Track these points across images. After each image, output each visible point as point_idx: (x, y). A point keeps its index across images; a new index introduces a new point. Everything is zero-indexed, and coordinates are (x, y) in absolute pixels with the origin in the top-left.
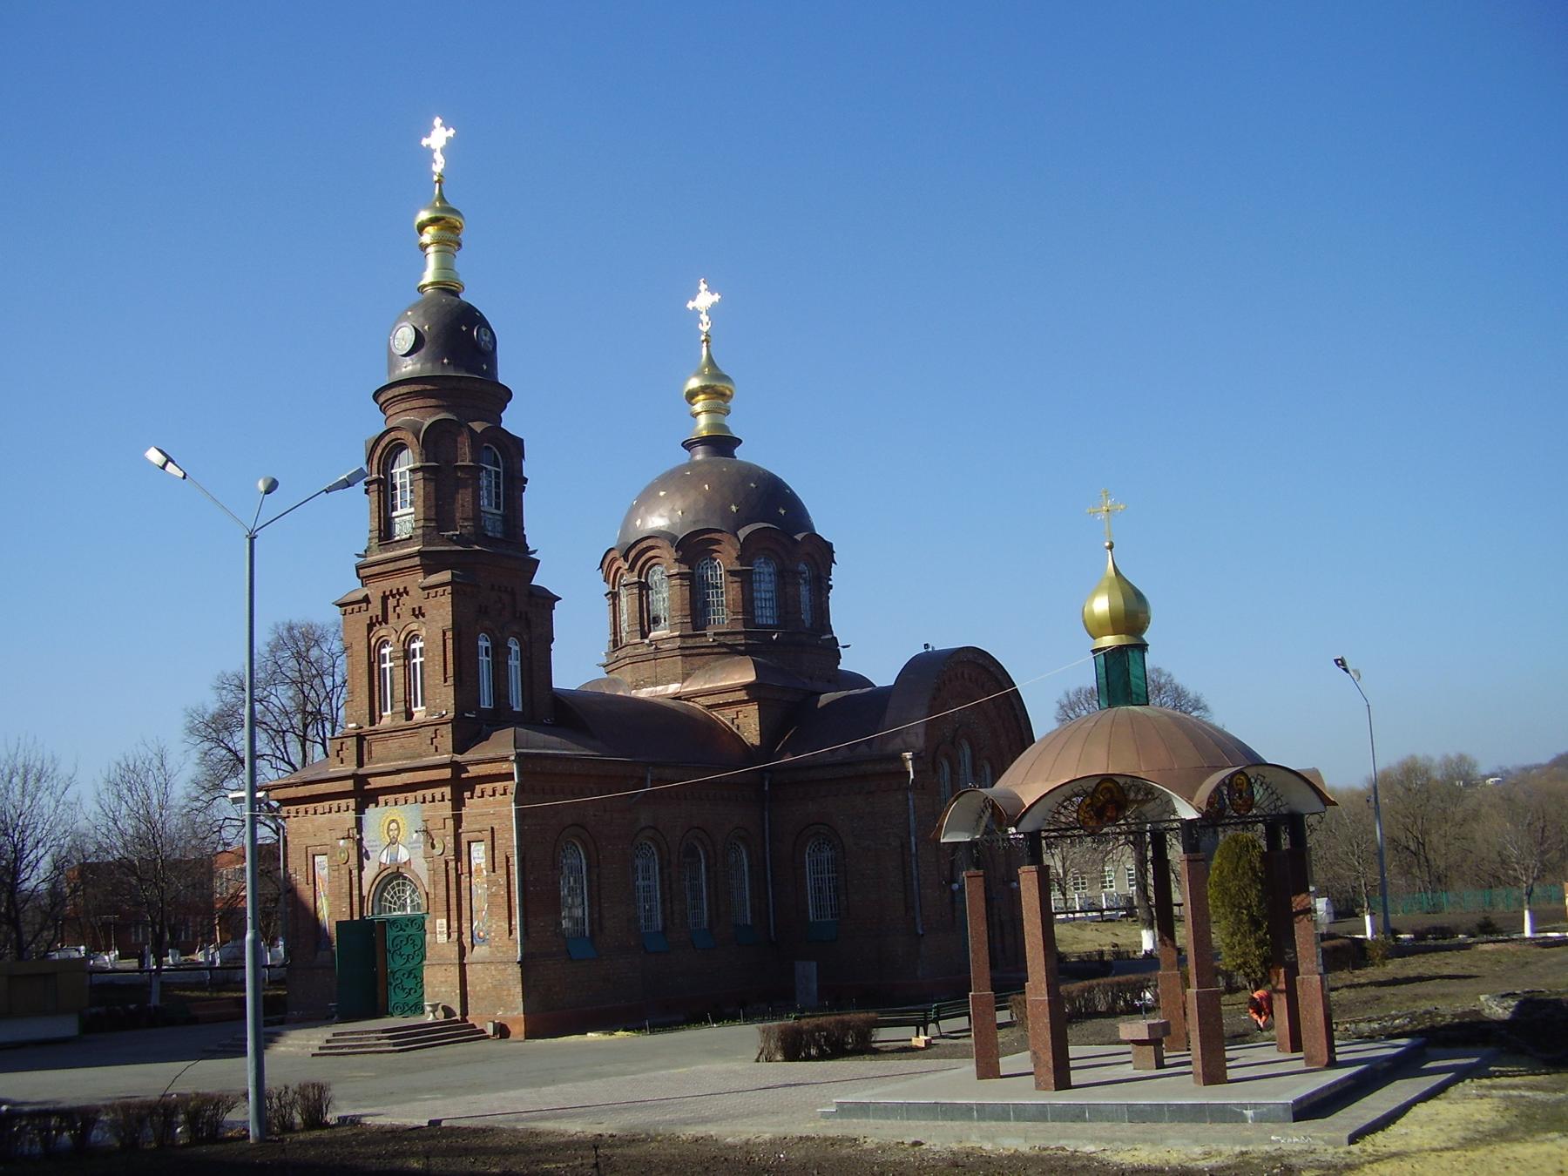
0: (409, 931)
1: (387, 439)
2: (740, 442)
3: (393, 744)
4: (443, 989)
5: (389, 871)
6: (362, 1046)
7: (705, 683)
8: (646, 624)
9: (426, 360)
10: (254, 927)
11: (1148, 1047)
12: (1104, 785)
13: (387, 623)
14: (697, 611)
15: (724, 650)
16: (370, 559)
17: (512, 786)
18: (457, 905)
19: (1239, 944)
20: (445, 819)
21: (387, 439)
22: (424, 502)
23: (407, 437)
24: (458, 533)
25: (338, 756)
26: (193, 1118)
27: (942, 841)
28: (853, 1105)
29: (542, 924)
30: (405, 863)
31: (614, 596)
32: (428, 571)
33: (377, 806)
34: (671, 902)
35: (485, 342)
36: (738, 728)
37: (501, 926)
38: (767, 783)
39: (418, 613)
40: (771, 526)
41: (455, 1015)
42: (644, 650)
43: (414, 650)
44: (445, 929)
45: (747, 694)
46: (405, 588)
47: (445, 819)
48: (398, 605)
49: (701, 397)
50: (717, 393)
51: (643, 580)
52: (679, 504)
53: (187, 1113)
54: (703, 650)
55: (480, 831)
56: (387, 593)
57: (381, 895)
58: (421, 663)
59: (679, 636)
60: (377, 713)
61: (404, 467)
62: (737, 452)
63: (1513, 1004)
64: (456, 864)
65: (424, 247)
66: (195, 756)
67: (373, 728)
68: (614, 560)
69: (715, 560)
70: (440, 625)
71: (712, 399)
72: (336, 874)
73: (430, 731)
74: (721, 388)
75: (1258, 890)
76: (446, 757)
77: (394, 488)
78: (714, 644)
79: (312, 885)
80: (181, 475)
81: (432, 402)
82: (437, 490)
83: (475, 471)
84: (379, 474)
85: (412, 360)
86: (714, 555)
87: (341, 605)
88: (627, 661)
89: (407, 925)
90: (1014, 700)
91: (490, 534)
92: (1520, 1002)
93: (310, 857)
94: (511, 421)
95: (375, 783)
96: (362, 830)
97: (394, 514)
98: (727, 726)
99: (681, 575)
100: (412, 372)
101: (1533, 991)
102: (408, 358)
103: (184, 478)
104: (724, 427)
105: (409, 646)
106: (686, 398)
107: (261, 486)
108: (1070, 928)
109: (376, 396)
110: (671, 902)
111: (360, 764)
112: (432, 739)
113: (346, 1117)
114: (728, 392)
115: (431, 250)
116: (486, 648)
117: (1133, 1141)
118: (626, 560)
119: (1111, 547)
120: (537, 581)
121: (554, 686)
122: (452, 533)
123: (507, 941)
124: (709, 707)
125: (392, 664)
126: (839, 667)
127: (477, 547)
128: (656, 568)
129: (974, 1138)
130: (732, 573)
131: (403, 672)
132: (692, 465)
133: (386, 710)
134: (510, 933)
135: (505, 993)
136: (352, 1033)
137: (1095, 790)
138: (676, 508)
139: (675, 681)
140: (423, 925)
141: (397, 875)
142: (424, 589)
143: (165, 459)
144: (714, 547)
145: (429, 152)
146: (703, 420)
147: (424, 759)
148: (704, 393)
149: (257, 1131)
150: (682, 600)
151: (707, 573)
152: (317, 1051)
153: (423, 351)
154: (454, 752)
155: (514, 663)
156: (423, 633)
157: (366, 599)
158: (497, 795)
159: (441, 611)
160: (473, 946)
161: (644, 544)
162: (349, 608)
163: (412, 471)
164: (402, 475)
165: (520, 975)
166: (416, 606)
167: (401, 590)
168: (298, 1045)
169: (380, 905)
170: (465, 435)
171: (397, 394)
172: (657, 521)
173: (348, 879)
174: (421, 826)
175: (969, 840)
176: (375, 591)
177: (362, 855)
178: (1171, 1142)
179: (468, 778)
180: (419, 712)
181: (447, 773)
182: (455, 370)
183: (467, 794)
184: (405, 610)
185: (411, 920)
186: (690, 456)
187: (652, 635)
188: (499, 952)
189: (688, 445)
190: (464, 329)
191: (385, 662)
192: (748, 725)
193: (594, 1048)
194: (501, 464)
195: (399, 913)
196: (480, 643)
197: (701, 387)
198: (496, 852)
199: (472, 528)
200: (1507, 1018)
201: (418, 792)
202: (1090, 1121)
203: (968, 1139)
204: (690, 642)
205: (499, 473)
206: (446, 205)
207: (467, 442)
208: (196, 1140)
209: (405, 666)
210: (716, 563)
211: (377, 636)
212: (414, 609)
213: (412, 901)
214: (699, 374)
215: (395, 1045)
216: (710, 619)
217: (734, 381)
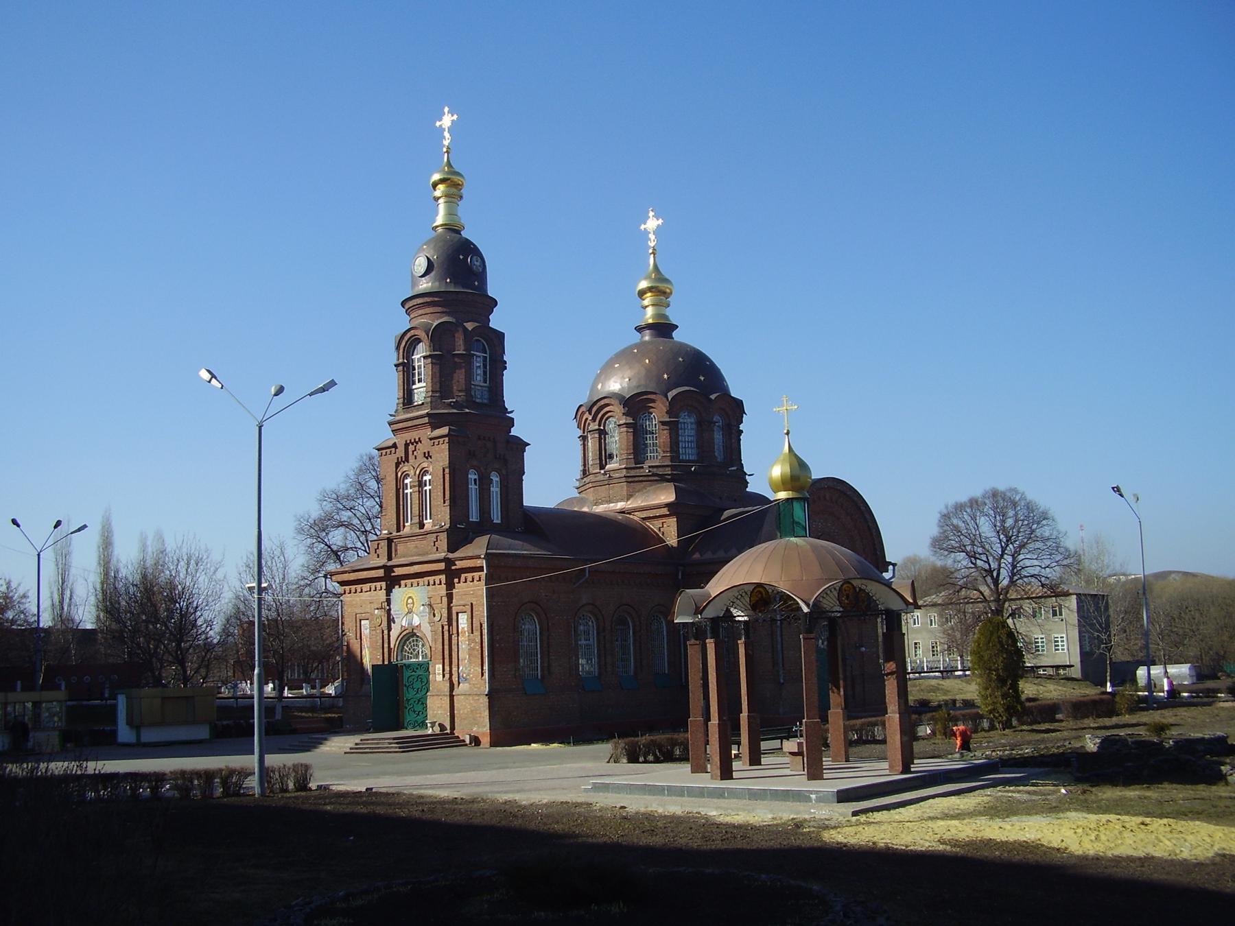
0: (419, 672)
1: (409, 335)
2: (677, 327)
3: (411, 545)
4: (439, 712)
5: (407, 631)
6: (379, 748)
7: (642, 502)
8: (603, 459)
9: (435, 280)
10: (259, 666)
11: (799, 757)
12: (758, 589)
13: (408, 462)
14: (638, 451)
15: (657, 478)
16: (398, 418)
17: (483, 574)
18: (449, 656)
19: (991, 696)
20: (442, 597)
21: (409, 335)
22: (432, 379)
23: (421, 334)
24: (454, 400)
25: (376, 552)
26: (225, 782)
27: (675, 621)
28: (601, 785)
29: (505, 669)
30: (417, 626)
31: (584, 438)
32: (434, 427)
33: (400, 587)
35: (476, 266)
36: (663, 535)
37: (477, 670)
38: (680, 574)
39: (427, 456)
40: (692, 389)
41: (446, 730)
42: (602, 478)
43: (426, 481)
44: (441, 672)
45: (669, 510)
46: (419, 439)
47: (442, 597)
48: (415, 450)
49: (649, 294)
50: (660, 291)
51: (602, 428)
52: (628, 373)
53: (221, 778)
54: (641, 478)
55: (464, 606)
56: (408, 442)
57: (403, 647)
58: (430, 490)
59: (625, 468)
60: (402, 524)
61: (420, 354)
62: (675, 334)
63: (1099, 741)
64: (449, 627)
65: (437, 199)
66: (303, 549)
67: (398, 534)
68: (583, 413)
69: (652, 414)
70: (441, 464)
71: (657, 296)
72: (374, 632)
73: (432, 537)
74: (663, 288)
75: (1004, 658)
76: (442, 555)
77: (414, 369)
78: (650, 474)
79: (359, 640)
80: (220, 386)
81: (439, 309)
82: (441, 371)
83: (468, 358)
84: (403, 359)
85: (425, 280)
86: (651, 410)
87: (378, 450)
88: (590, 485)
89: (417, 669)
91: (478, 401)
92: (1102, 740)
93: (358, 620)
95: (398, 571)
96: (390, 603)
97: (414, 387)
98: (655, 532)
99: (627, 425)
100: (425, 289)
101: (1133, 734)
102: (423, 279)
103: (222, 388)
104: (665, 317)
105: (422, 478)
106: (639, 296)
107: (273, 391)
108: (960, 682)
109: (403, 304)
111: (390, 558)
112: (434, 542)
113: (322, 786)
114: (668, 291)
115: (441, 201)
116: (475, 480)
117: (738, 809)
118: (590, 414)
119: (788, 433)
120: (514, 432)
121: (525, 504)
122: (451, 400)
123: (480, 680)
124: (644, 519)
125: (411, 490)
126: (747, 490)
127: (467, 411)
128: (611, 419)
129: (654, 805)
130: (663, 423)
131: (418, 495)
132: (643, 344)
133: (407, 522)
134: (482, 675)
135: (479, 715)
136: (373, 739)
138: (625, 376)
139: (622, 500)
140: (428, 669)
141: (413, 634)
142: (431, 439)
143: (210, 376)
144: (650, 405)
145: (442, 129)
146: (650, 311)
147: (430, 556)
148: (651, 292)
149: (259, 790)
150: (628, 442)
151: (646, 423)
152: (348, 750)
153: (433, 274)
154: (448, 551)
155: (495, 489)
156: (431, 469)
157: (395, 446)
158: (468, 582)
159: (442, 454)
160: (459, 683)
161: (602, 403)
162: (384, 451)
163: (424, 357)
164: (419, 360)
165: (487, 704)
166: (426, 451)
167: (417, 440)
168: (338, 746)
169: (402, 654)
170: (460, 332)
171: (415, 304)
172: (616, 385)
173: (381, 636)
174: (426, 601)
175: (691, 621)
176: (400, 440)
177: (390, 620)
178: (758, 811)
179: (456, 569)
180: (428, 522)
181: (442, 566)
182: (455, 287)
183: (456, 580)
184: (419, 453)
185: (420, 665)
186: (640, 337)
187: (607, 467)
188: (475, 688)
189: (640, 329)
190: (461, 257)
191: (407, 489)
192: (670, 532)
193: (535, 752)
194: (488, 352)
195: (414, 660)
196: (470, 476)
197: (648, 287)
198: (474, 620)
199: (464, 397)
200: (1095, 751)
201: (425, 578)
202: (727, 798)
203: (651, 806)
204: (633, 473)
205: (486, 357)
206: (452, 170)
207: (462, 337)
208: (226, 793)
209: (419, 492)
210: (652, 416)
212: (425, 453)
213: (422, 652)
214: (647, 278)
215: (400, 748)
216: (647, 456)
217: (672, 281)
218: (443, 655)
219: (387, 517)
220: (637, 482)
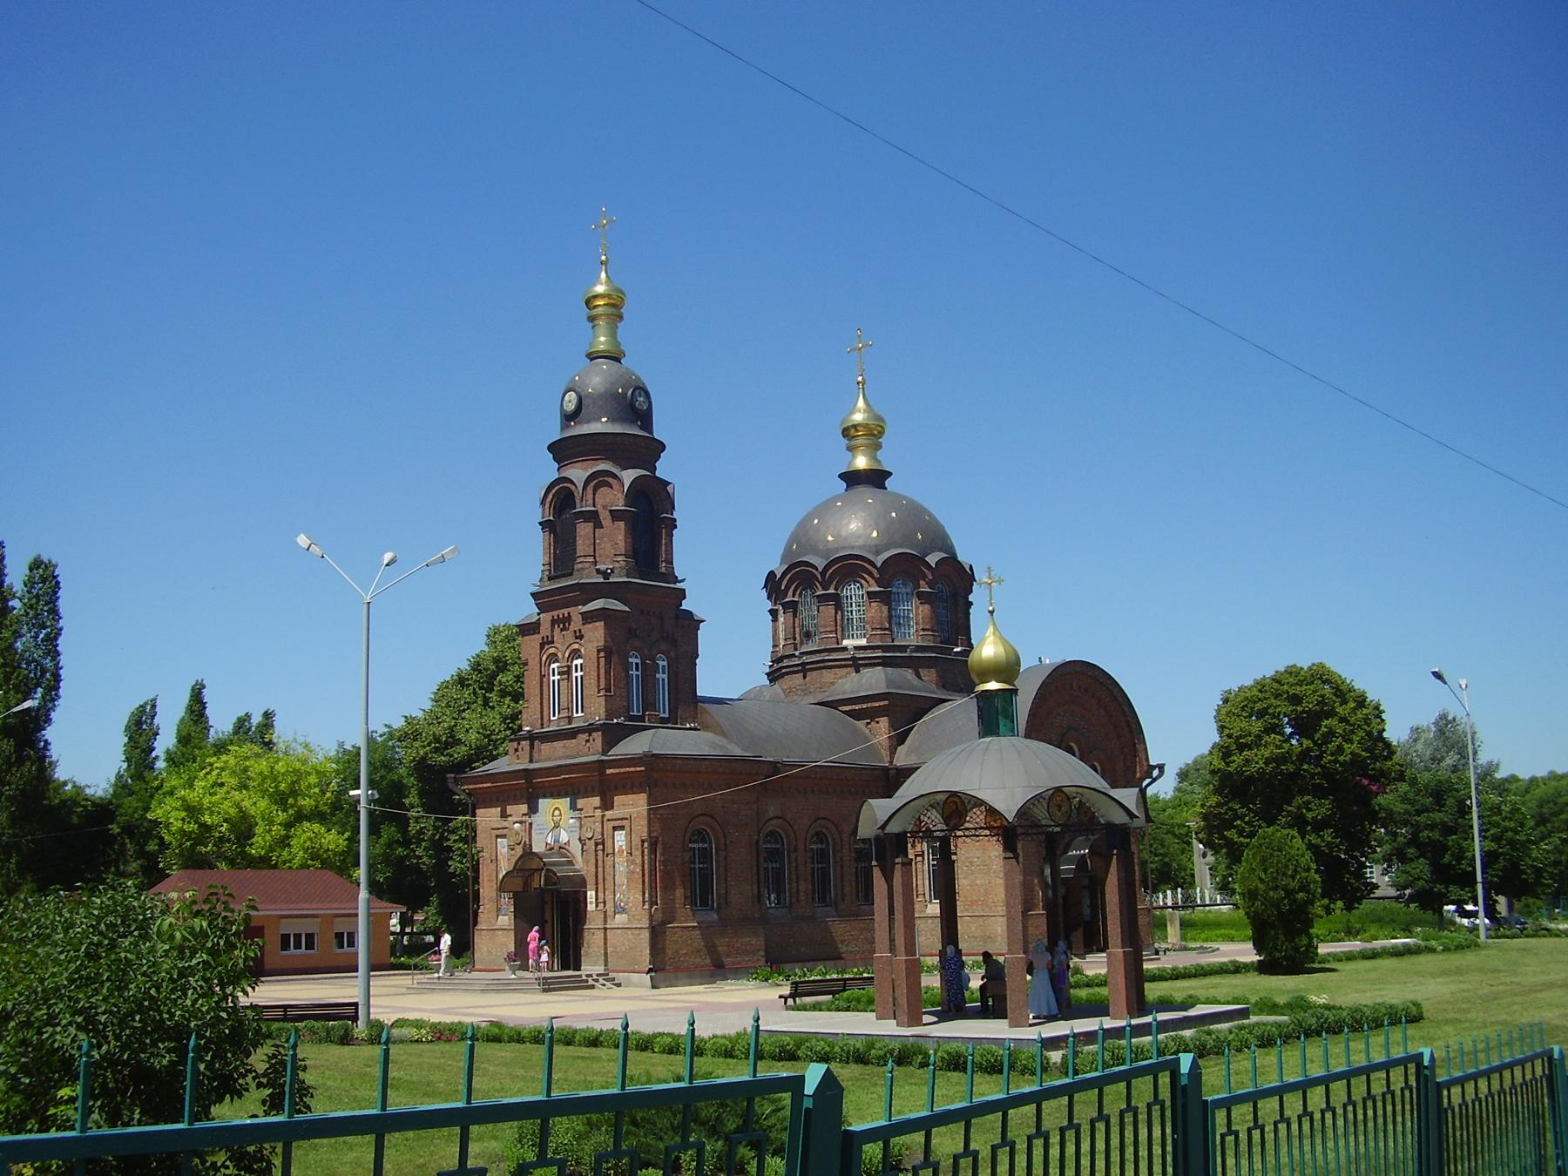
34: (797, 882)
62: (887, 483)
70: (595, 645)
90: (1126, 709)
110: (797, 882)
116: (637, 664)
120: (685, 605)
137: (945, 802)
211: (547, 653)
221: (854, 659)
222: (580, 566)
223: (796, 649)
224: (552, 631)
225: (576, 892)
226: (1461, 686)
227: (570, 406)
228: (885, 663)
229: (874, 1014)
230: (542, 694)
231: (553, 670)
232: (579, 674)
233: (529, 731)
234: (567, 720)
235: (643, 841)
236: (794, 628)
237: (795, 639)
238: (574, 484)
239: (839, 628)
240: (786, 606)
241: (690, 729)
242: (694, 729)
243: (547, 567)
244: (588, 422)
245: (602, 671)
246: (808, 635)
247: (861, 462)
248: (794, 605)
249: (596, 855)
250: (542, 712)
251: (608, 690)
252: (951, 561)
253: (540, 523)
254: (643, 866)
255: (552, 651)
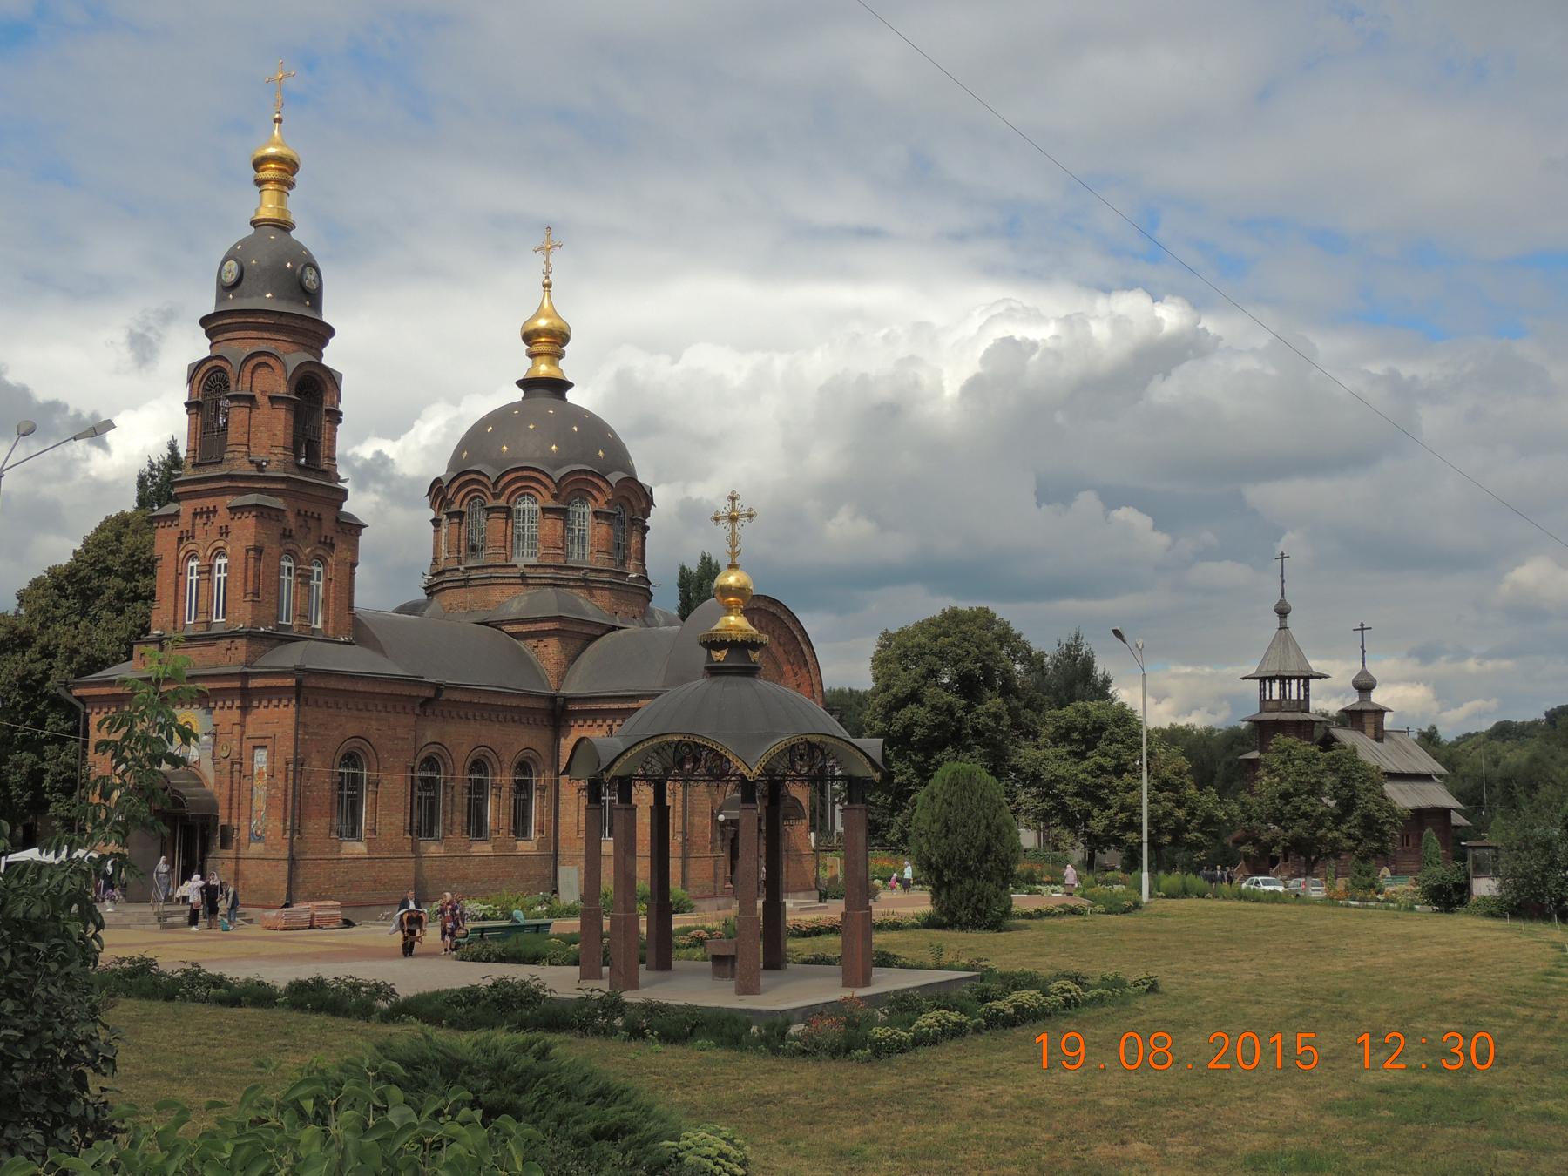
58: (225, 578)
62: (292, 233)
70: (244, 544)
71: (280, 169)
94: (331, 356)
116: (289, 569)
120: (347, 507)
166: (223, 525)
211: (186, 549)
218: (231, 804)
219: (161, 611)
220: (506, 584)
221: (523, 577)
222: (231, 455)
223: (460, 563)
224: (193, 525)
225: (206, 817)
226: (1137, 646)
227: (230, 278)
228: (555, 584)
229: (577, 969)
230: (176, 594)
231: (192, 568)
232: (223, 575)
233: (160, 635)
234: (205, 625)
235: (287, 763)
236: (459, 540)
237: (459, 552)
238: (227, 360)
239: (509, 544)
240: (450, 516)
241: (344, 643)
242: (349, 643)
243: (191, 454)
244: (250, 296)
245: (250, 573)
246: (473, 549)
247: (544, 369)
248: (460, 515)
249: (232, 777)
250: (175, 614)
251: (256, 594)
252: (632, 483)
253: (186, 404)
254: (286, 791)
255: (192, 547)
